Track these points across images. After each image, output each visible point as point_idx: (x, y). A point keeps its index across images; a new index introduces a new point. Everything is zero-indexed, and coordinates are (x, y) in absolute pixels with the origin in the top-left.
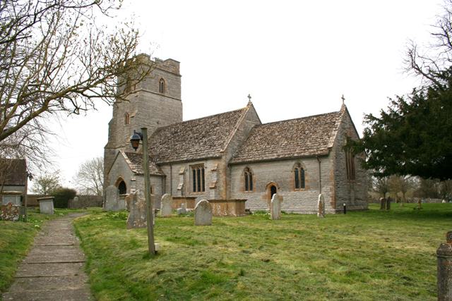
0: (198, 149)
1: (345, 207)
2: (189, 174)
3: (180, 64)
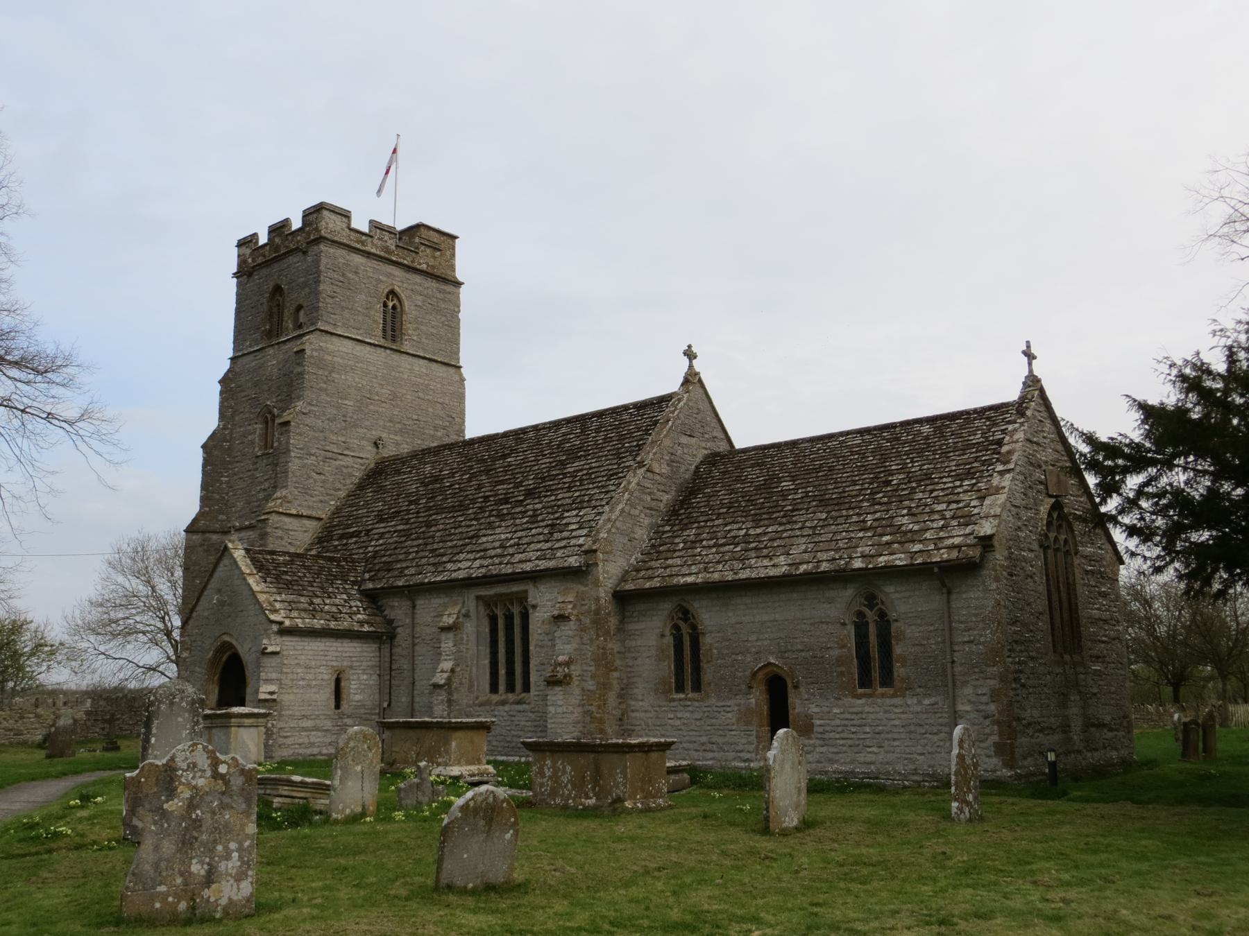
0: (509, 546)
1: (1053, 765)
2: (474, 630)
3: (463, 289)
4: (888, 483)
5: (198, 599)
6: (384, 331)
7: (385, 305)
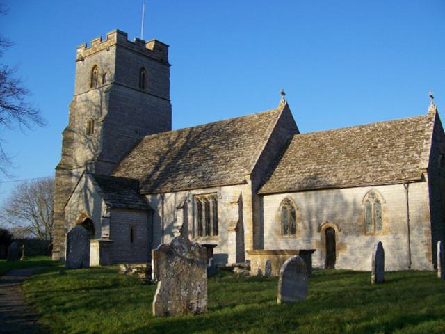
4: (376, 147)
5: (228, 185)
6: (140, 84)
7: (140, 73)
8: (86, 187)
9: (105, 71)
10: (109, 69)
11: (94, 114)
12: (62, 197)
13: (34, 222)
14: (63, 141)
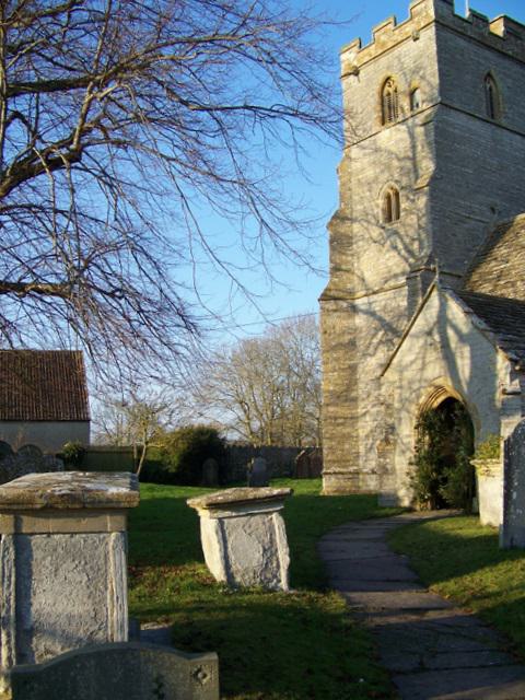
8: (443, 320)
9: (415, 83)
10: (423, 78)
11: (396, 176)
12: (337, 360)
13: (241, 414)
14: (331, 242)
